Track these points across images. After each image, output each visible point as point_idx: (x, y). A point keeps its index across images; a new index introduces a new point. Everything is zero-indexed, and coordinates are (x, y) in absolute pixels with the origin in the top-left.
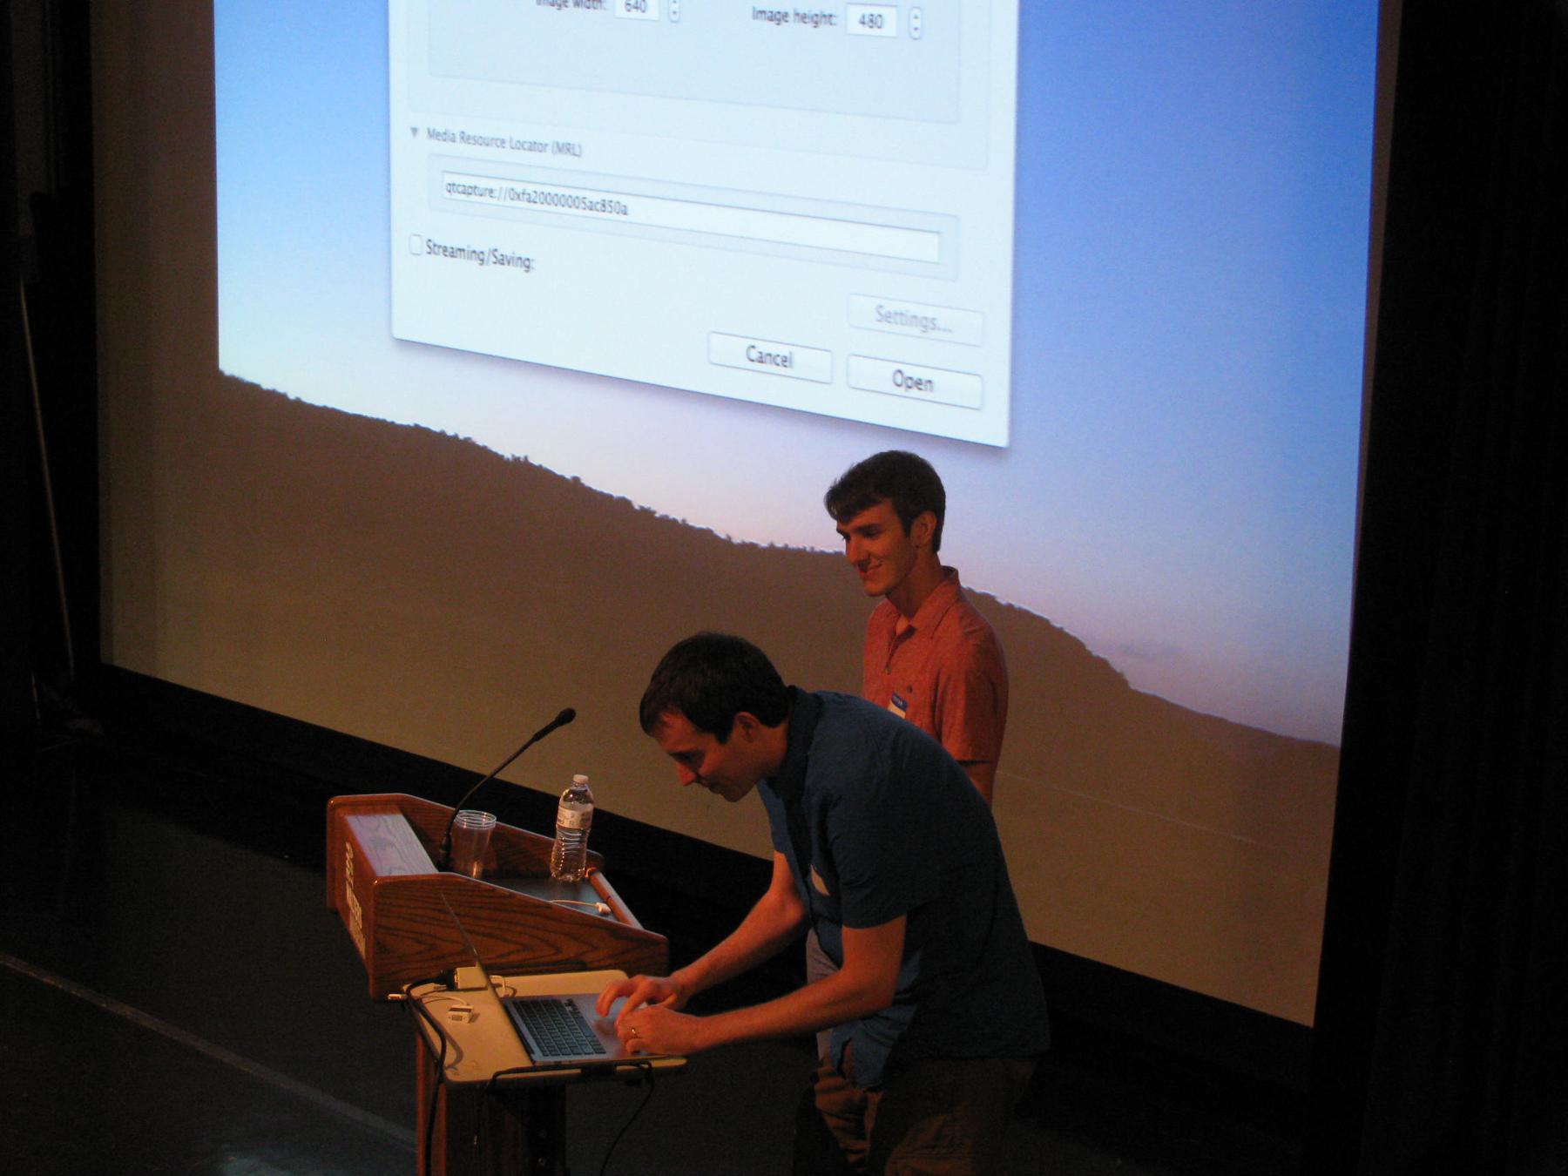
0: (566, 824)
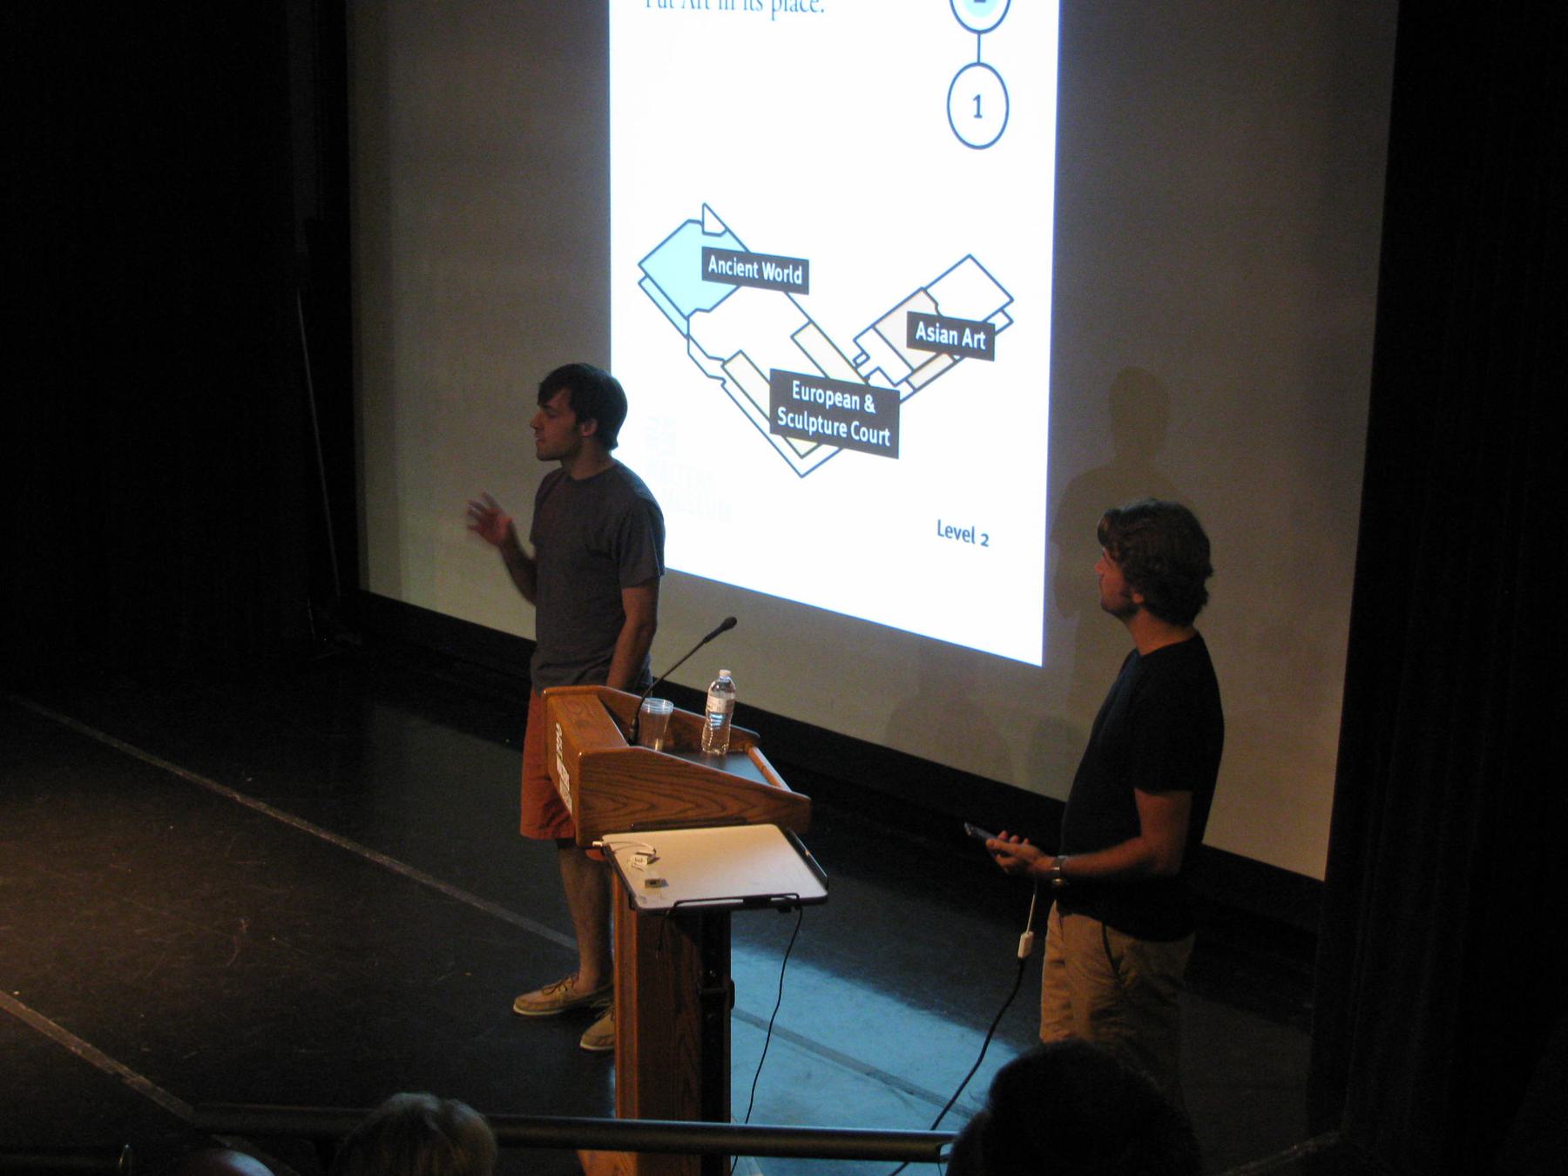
0: (714, 709)
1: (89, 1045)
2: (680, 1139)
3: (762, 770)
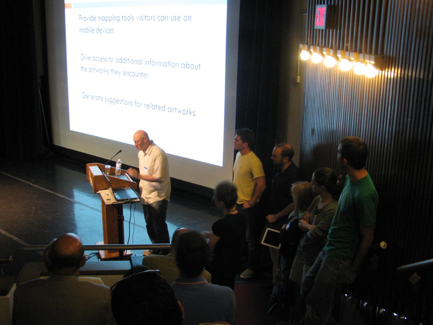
1: (6, 232)
2: (114, 248)
3: (127, 177)
